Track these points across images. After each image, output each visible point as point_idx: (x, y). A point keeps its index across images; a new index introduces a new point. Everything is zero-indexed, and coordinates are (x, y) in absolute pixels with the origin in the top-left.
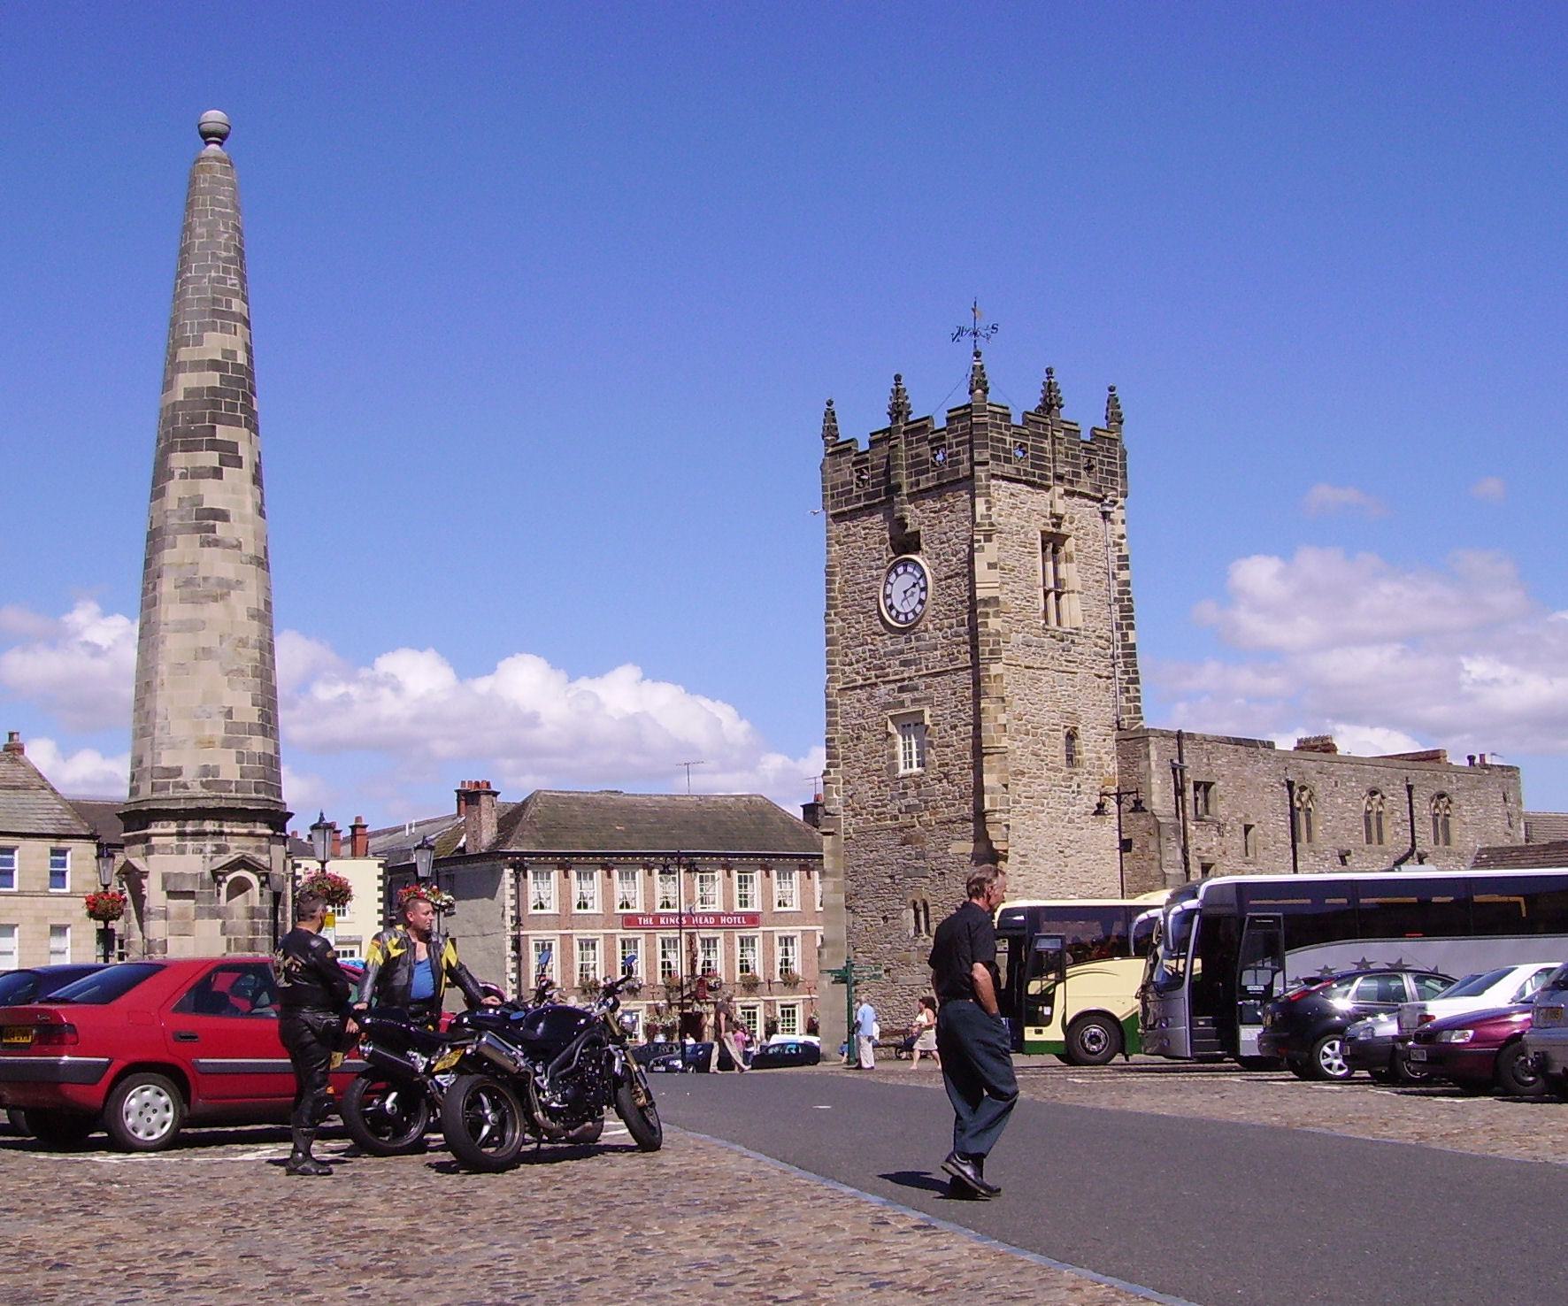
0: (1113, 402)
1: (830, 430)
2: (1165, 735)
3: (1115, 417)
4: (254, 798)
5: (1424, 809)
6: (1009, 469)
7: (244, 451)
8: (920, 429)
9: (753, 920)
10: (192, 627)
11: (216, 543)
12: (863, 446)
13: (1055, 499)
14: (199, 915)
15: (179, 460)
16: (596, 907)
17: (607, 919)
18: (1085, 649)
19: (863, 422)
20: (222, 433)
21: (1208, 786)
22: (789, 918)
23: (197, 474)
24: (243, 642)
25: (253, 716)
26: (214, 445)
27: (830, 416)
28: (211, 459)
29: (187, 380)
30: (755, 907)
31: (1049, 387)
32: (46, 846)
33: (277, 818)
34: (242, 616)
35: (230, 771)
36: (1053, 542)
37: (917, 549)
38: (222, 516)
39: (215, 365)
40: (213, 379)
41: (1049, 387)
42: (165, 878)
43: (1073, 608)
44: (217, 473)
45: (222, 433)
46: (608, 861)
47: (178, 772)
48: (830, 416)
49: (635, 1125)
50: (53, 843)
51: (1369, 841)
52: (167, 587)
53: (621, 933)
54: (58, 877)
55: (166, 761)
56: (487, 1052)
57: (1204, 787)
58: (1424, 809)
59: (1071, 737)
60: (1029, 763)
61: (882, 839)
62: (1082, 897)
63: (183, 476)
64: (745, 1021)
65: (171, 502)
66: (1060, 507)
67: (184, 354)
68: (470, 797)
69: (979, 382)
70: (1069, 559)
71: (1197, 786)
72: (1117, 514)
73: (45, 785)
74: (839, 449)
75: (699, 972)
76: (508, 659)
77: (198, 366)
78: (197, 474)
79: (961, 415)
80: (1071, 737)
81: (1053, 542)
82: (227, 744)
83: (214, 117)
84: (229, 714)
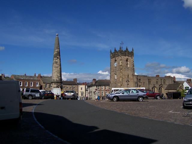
0: (133, 49)
3: (133, 50)
4: (60, 81)
5: (162, 81)
6: (123, 55)
10: (55, 70)
13: (127, 57)
15: (55, 58)
16: (103, 89)
17: (104, 90)
19: (113, 51)
20: (57, 56)
21: (140, 79)
23: (55, 59)
25: (59, 76)
28: (56, 58)
29: (55, 53)
31: (127, 48)
32: (49, 84)
35: (58, 80)
38: (57, 62)
40: (57, 53)
43: (129, 66)
44: (57, 59)
45: (57, 56)
49: (47, 78)
51: (157, 83)
52: (54, 67)
59: (128, 76)
60: (124, 78)
64: (141, 109)
66: (127, 58)
67: (55, 51)
71: (139, 79)
76: (65, 80)
77: (56, 52)
78: (55, 59)
80: (128, 76)
81: (127, 60)
83: (57, 34)
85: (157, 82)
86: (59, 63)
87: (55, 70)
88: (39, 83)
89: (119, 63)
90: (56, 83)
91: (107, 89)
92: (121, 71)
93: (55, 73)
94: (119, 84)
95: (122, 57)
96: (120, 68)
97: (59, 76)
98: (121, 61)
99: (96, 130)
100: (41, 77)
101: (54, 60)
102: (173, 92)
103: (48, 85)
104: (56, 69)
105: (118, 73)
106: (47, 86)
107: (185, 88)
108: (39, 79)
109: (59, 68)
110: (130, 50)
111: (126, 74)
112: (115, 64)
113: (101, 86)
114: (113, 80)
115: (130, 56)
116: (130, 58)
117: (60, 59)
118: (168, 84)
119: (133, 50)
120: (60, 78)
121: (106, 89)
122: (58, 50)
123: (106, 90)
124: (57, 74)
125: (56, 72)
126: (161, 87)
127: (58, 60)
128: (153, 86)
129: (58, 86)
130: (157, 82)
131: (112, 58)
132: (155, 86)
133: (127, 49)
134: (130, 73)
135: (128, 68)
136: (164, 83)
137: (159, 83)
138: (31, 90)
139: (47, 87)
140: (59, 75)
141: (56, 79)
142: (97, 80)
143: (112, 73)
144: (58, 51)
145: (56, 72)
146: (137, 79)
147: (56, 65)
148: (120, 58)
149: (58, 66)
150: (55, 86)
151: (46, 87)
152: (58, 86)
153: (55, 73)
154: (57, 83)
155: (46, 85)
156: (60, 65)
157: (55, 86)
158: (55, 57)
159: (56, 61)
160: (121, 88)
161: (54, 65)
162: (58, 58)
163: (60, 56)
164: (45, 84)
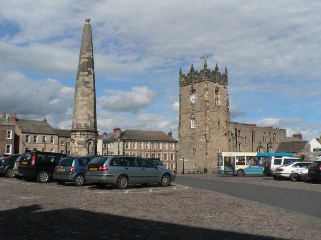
1: (181, 73)
2: (234, 123)
4: (93, 129)
7: (92, 72)
8: (196, 73)
9: (160, 151)
11: (87, 87)
12: (186, 75)
13: (217, 85)
14: (84, 148)
15: (82, 73)
18: (222, 109)
19: (186, 71)
20: (89, 69)
22: (166, 151)
24: (91, 103)
25: (93, 115)
26: (87, 71)
27: (181, 70)
28: (86, 73)
30: (161, 149)
31: (217, 67)
32: (50, 136)
33: (96, 132)
34: (91, 98)
35: (89, 124)
36: (217, 91)
37: (195, 92)
38: (88, 82)
39: (88, 58)
40: (87, 60)
41: (217, 67)
42: (78, 142)
43: (219, 103)
44: (88, 76)
45: (89, 69)
46: (145, 141)
47: (81, 124)
48: (181, 70)
50: (51, 136)
52: (79, 94)
53: (140, 152)
54: (52, 141)
55: (79, 122)
56: (69, 167)
57: (239, 131)
58: (272, 136)
60: (212, 127)
61: (188, 138)
62: (290, 157)
63: (82, 76)
65: (80, 80)
66: (218, 86)
68: (116, 130)
69: (205, 66)
70: (219, 94)
72: (227, 87)
73: (50, 126)
74: (182, 76)
75: (305, 171)
79: (202, 71)
81: (217, 91)
82: (88, 120)
84: (89, 115)
85: (264, 138)
86: (91, 85)
87: (83, 100)
88: (14, 132)
89: (203, 96)
90: (84, 131)
91: (142, 148)
92: (208, 111)
93: (82, 107)
94: (200, 140)
95: (209, 83)
96: (205, 106)
97: (92, 115)
98: (207, 93)
99: (38, 211)
100: (17, 120)
101: (81, 78)
102: (247, 157)
103: (31, 137)
104: (86, 98)
105: (198, 116)
106: (29, 138)
107: (314, 150)
108: (13, 123)
109: (92, 96)
110: (222, 71)
111: (216, 119)
112: (193, 98)
113: (157, 142)
114: (185, 130)
115: (222, 82)
116: (221, 87)
117: (94, 77)
118: (279, 141)
119: (226, 70)
120: (93, 120)
121: (140, 147)
122: (90, 54)
123: (141, 151)
124: (87, 112)
125: (86, 105)
126: (270, 146)
127: (89, 79)
128: (258, 145)
129: (90, 139)
130: (264, 138)
131: (182, 84)
132: (262, 145)
133: (217, 69)
134: (223, 118)
135: (219, 107)
136: (275, 139)
137: (267, 140)
138: (285, 159)
139: (29, 141)
140: (91, 113)
141: (85, 122)
142: (123, 130)
143: (182, 116)
144: (90, 56)
145: (86, 105)
146: (236, 130)
147: (87, 90)
148: (206, 86)
149: (89, 92)
150: (83, 139)
151: (27, 140)
152: (90, 139)
153: (82, 107)
154: (87, 131)
155: (27, 137)
156: (94, 90)
157: (83, 139)
158: (83, 71)
159: (87, 79)
160: (240, 151)
161: (79, 89)
162: (89, 72)
163: (93, 69)
164: (25, 135)
